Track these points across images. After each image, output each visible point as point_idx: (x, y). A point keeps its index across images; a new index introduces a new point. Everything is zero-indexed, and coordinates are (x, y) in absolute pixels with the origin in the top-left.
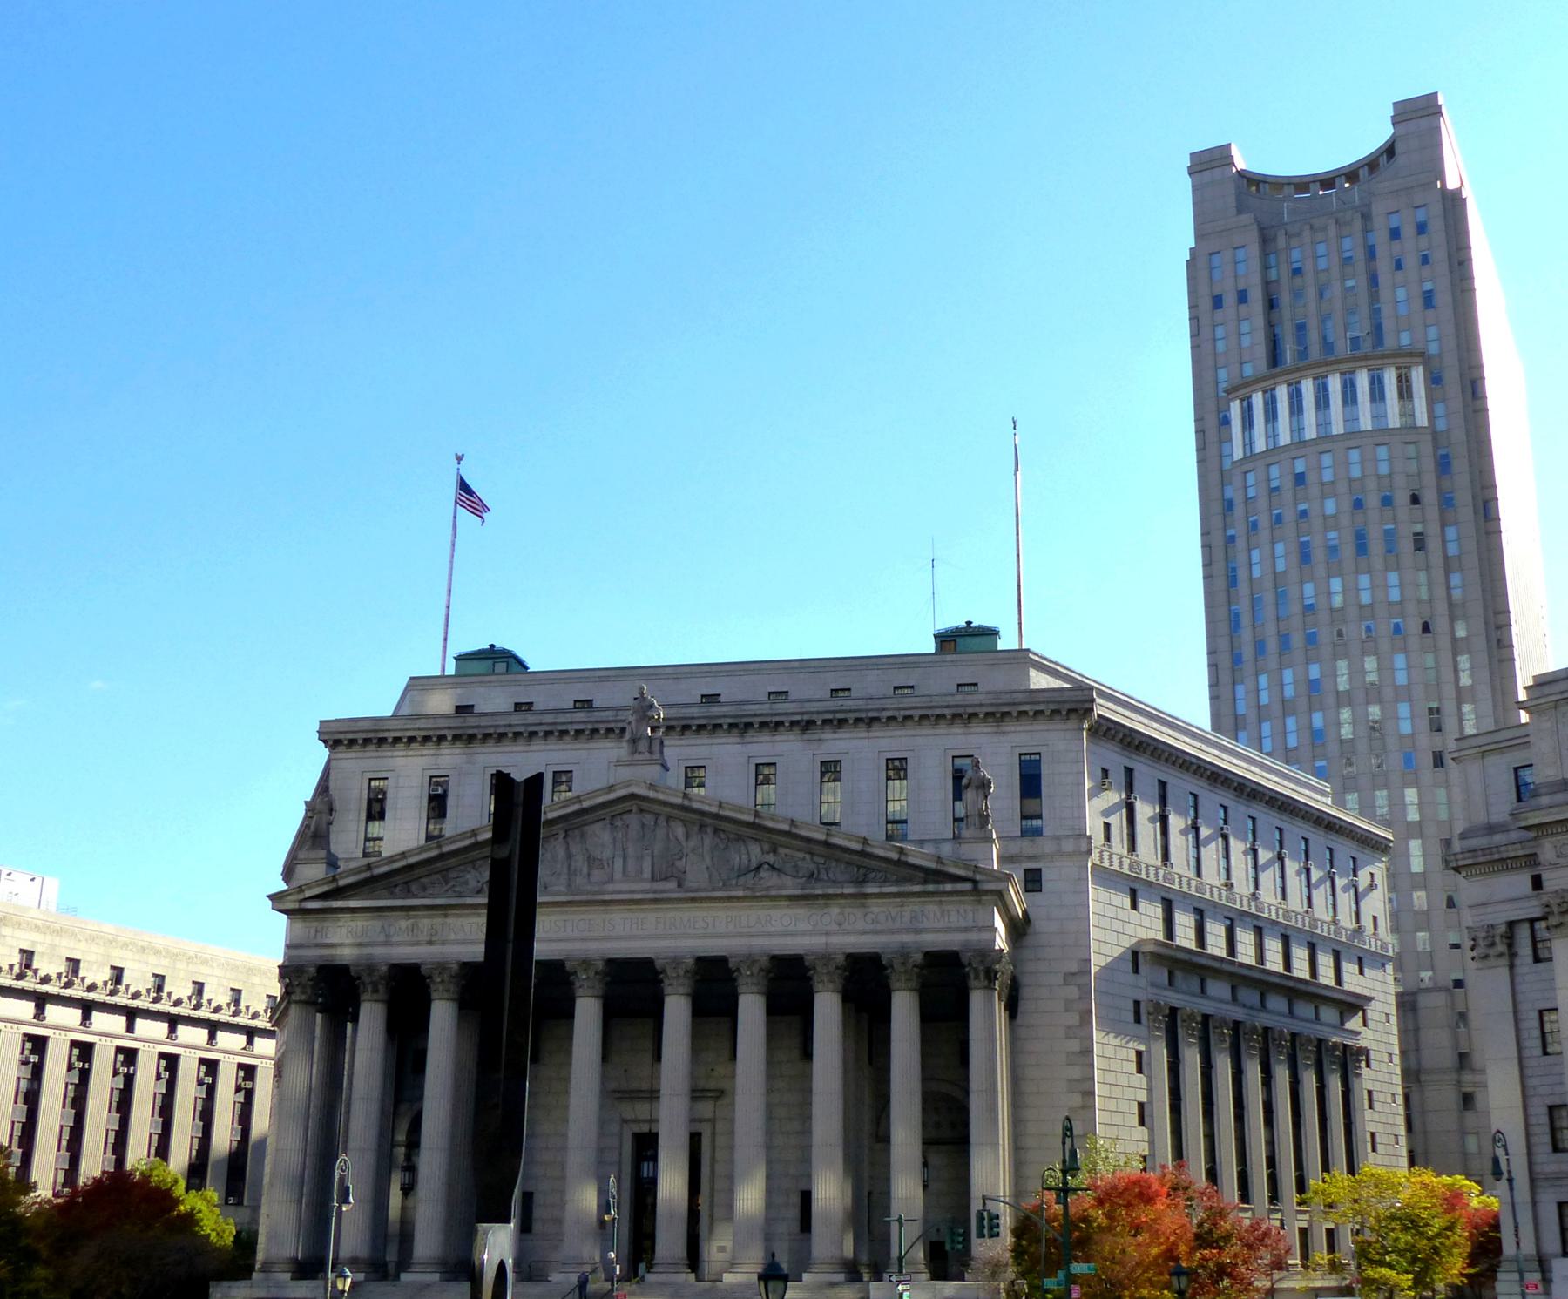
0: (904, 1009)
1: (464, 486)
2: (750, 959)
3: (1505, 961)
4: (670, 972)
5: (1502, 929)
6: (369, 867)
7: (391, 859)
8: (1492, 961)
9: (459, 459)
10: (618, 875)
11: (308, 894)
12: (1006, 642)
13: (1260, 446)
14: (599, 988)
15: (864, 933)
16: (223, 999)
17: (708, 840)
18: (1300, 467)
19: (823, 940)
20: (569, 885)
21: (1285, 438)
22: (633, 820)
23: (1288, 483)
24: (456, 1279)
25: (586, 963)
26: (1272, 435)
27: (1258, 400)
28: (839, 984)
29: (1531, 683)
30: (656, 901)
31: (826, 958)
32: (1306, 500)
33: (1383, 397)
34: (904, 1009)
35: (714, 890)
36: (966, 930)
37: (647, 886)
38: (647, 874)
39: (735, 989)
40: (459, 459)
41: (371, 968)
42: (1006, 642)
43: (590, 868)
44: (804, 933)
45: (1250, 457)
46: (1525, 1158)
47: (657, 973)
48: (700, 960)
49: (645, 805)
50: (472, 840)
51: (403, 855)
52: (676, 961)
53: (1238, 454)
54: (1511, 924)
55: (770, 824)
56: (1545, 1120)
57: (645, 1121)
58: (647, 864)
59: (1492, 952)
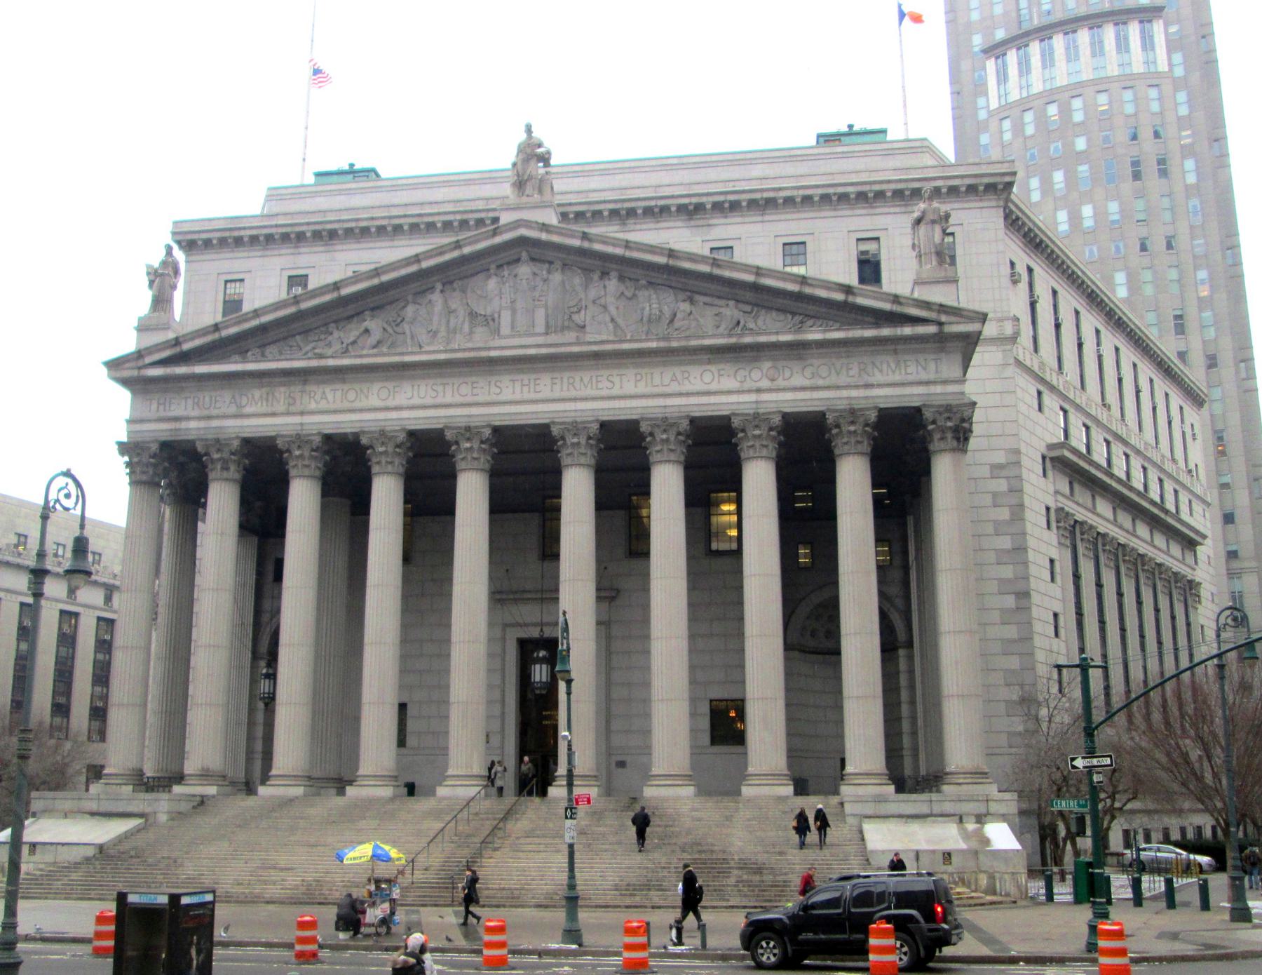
0: (853, 486)
2: (666, 423)
4: (571, 440)
6: (296, 300)
7: (256, 313)
10: (505, 330)
11: (148, 360)
14: (485, 461)
15: (803, 389)
17: (613, 284)
19: (753, 397)
20: (513, 328)
22: (524, 270)
25: (469, 431)
28: (866, 447)
31: (757, 418)
35: (621, 341)
36: (928, 383)
37: (541, 340)
38: (540, 328)
39: (646, 458)
41: (219, 444)
43: (472, 325)
44: (729, 392)
46: (1095, 602)
47: (554, 441)
48: (605, 426)
49: (536, 252)
50: (335, 295)
51: (336, 286)
52: (576, 427)
55: (687, 265)
57: (535, 625)
58: (540, 315)
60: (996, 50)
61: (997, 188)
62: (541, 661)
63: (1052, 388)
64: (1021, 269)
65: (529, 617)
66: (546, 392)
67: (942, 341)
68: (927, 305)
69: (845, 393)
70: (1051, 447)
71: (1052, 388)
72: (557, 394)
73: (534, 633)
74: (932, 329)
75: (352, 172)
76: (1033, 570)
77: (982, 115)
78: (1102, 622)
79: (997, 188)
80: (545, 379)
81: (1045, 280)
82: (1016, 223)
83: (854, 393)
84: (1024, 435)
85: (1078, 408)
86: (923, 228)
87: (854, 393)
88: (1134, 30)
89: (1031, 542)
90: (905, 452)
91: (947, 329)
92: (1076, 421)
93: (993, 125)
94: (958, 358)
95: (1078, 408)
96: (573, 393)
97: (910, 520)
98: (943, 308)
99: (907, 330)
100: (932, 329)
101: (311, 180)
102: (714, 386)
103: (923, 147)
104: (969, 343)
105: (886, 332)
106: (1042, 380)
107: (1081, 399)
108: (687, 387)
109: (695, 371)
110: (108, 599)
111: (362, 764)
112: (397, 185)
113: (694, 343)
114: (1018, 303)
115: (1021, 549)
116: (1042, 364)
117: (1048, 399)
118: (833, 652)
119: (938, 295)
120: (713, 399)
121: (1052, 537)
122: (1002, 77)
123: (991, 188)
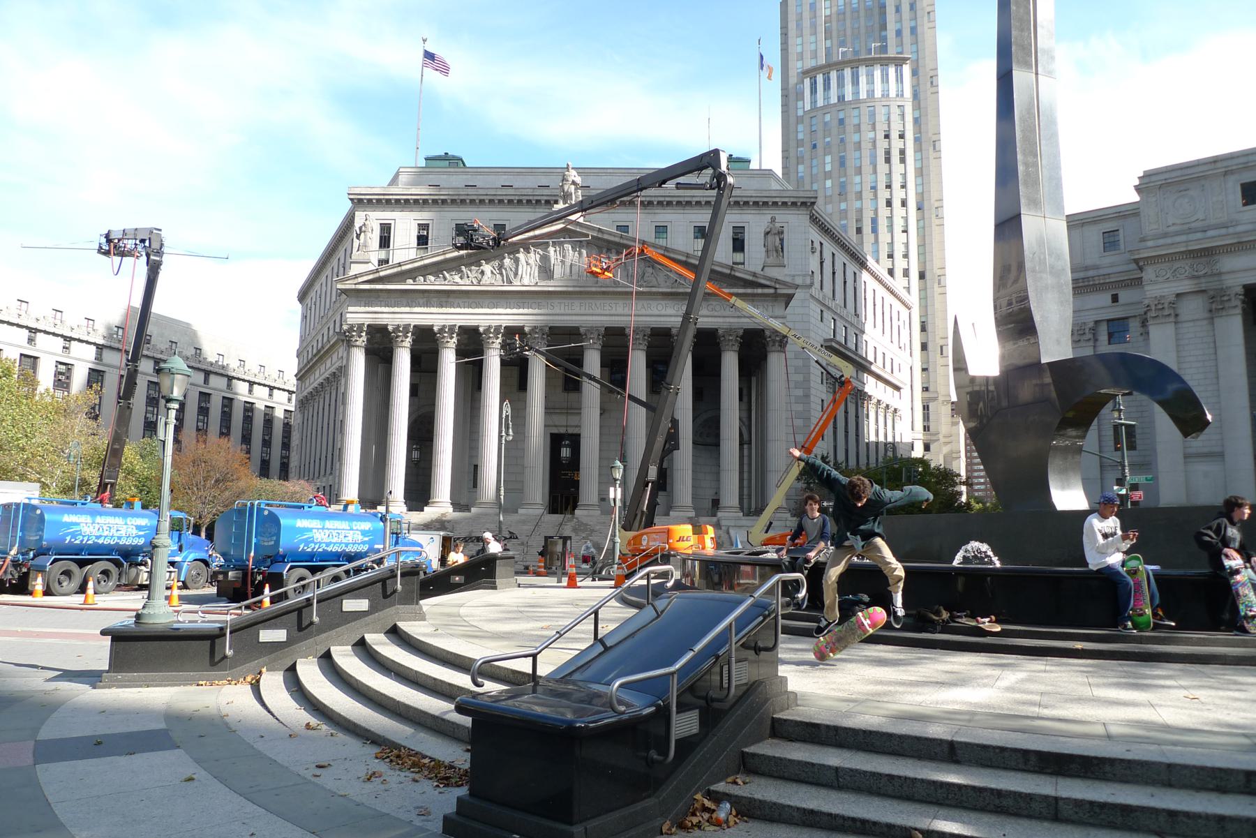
0: (730, 364)
1: (429, 56)
3: (1091, 343)
5: (1092, 325)
8: (1082, 344)
9: (425, 41)
11: (360, 280)
12: (754, 165)
13: (820, 103)
16: (256, 370)
18: (841, 115)
21: (834, 99)
23: (835, 123)
24: (795, 694)
26: (827, 98)
27: (820, 78)
29: (1137, 182)
30: (604, 293)
32: (830, 136)
33: (888, 81)
34: (730, 364)
40: (425, 41)
42: (754, 165)
45: (814, 108)
53: (808, 107)
54: (1097, 322)
56: (1111, 432)
59: (1083, 338)
60: (810, 73)
61: (807, 204)
62: (566, 446)
63: (829, 308)
64: (817, 245)
65: (563, 424)
66: (577, 311)
67: (776, 296)
68: (770, 279)
69: (728, 320)
70: (826, 340)
71: (829, 308)
72: (583, 312)
73: (562, 431)
74: (772, 291)
75: (446, 157)
76: (813, 405)
77: (800, 113)
78: (846, 432)
79: (807, 204)
80: (577, 303)
81: (829, 248)
82: (815, 220)
83: (732, 320)
84: (812, 334)
85: (842, 317)
86: (770, 237)
87: (732, 320)
88: (892, 70)
89: (813, 391)
90: (756, 349)
91: (779, 291)
92: (840, 324)
93: (807, 120)
94: (783, 305)
95: (842, 317)
96: (591, 312)
97: (754, 380)
98: (777, 281)
99: (760, 291)
100: (772, 291)
101: (422, 163)
102: (663, 312)
103: (769, 174)
104: (790, 297)
105: (749, 291)
106: (824, 305)
107: (844, 313)
108: (649, 312)
109: (654, 303)
110: (206, 381)
111: (1063, 488)
112: (478, 171)
113: (654, 290)
114: (814, 264)
115: (807, 396)
116: (824, 296)
117: (827, 315)
118: (717, 445)
119: (774, 273)
120: (662, 319)
121: (824, 388)
122: (814, 90)
123: (804, 204)
